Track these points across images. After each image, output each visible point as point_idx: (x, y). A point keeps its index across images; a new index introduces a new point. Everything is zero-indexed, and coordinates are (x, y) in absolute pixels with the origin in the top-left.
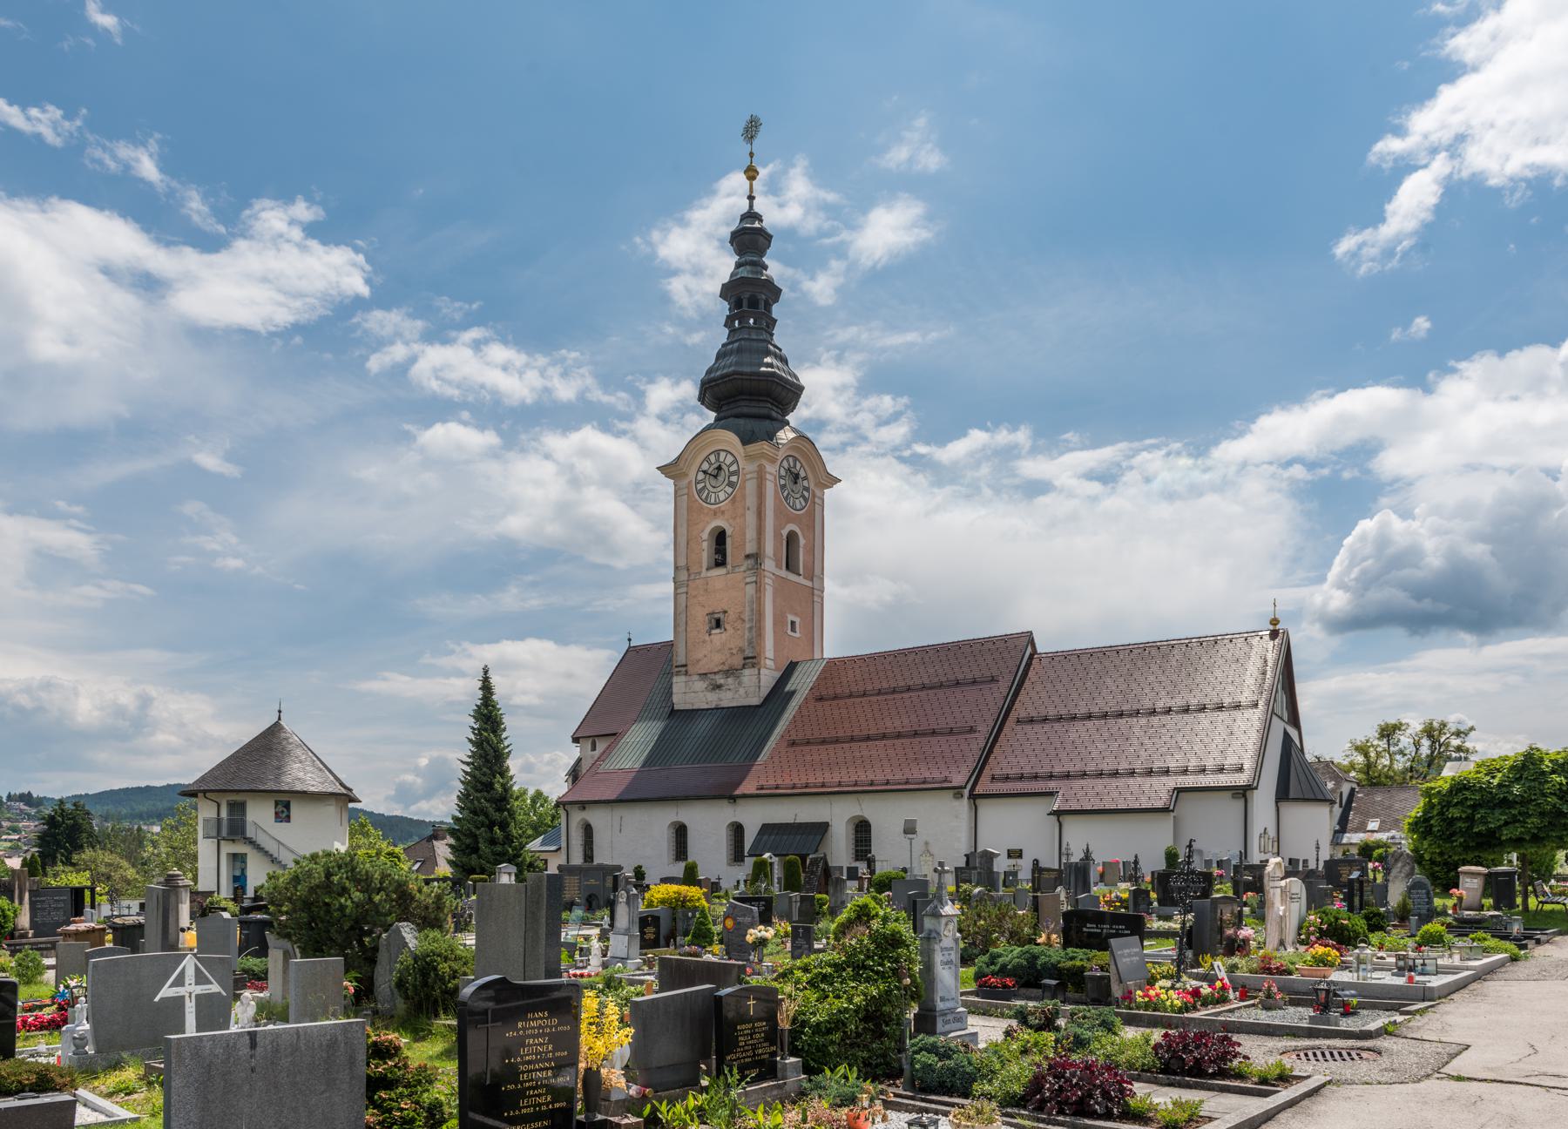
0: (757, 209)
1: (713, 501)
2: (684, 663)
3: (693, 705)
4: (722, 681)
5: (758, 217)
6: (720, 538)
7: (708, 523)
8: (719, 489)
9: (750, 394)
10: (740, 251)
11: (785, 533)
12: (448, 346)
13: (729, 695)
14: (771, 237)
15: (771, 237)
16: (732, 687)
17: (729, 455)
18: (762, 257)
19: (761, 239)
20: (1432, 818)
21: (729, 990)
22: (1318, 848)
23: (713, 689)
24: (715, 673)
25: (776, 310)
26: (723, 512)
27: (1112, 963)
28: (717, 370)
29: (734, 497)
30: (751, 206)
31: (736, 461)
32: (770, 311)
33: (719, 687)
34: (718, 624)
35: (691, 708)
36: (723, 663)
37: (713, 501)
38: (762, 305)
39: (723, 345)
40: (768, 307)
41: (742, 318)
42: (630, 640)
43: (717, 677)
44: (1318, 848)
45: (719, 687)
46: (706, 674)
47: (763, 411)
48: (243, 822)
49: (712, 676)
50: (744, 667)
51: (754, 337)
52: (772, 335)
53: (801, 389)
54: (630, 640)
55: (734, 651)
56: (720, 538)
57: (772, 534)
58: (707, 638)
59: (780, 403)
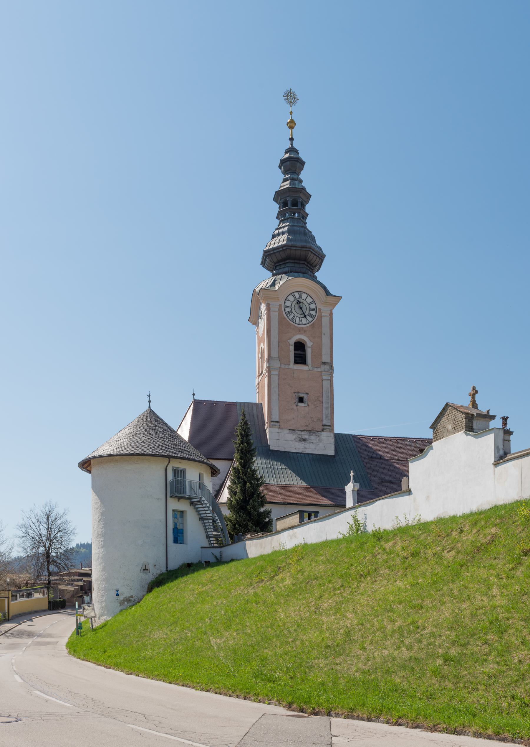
0: (295, 146)
2: (277, 420)
3: (284, 448)
4: (307, 437)
5: (296, 152)
6: (300, 346)
7: (294, 335)
9: (295, 259)
11: (292, 342)
13: (312, 446)
16: (314, 441)
17: (309, 297)
18: (298, 175)
19: (298, 164)
20: (88, 647)
23: (300, 441)
24: (301, 431)
25: (308, 208)
26: (305, 331)
29: (313, 324)
30: (292, 144)
31: (313, 302)
32: (304, 208)
33: (304, 440)
34: (301, 400)
35: (283, 450)
36: (307, 426)
37: (297, 322)
38: (299, 204)
40: (303, 206)
42: (194, 395)
43: (303, 433)
45: (304, 440)
46: (294, 430)
48: (184, 482)
49: (299, 432)
50: (323, 430)
51: (296, 224)
52: (306, 223)
54: (194, 395)
55: (315, 420)
56: (300, 346)
58: (295, 407)
59: (311, 265)
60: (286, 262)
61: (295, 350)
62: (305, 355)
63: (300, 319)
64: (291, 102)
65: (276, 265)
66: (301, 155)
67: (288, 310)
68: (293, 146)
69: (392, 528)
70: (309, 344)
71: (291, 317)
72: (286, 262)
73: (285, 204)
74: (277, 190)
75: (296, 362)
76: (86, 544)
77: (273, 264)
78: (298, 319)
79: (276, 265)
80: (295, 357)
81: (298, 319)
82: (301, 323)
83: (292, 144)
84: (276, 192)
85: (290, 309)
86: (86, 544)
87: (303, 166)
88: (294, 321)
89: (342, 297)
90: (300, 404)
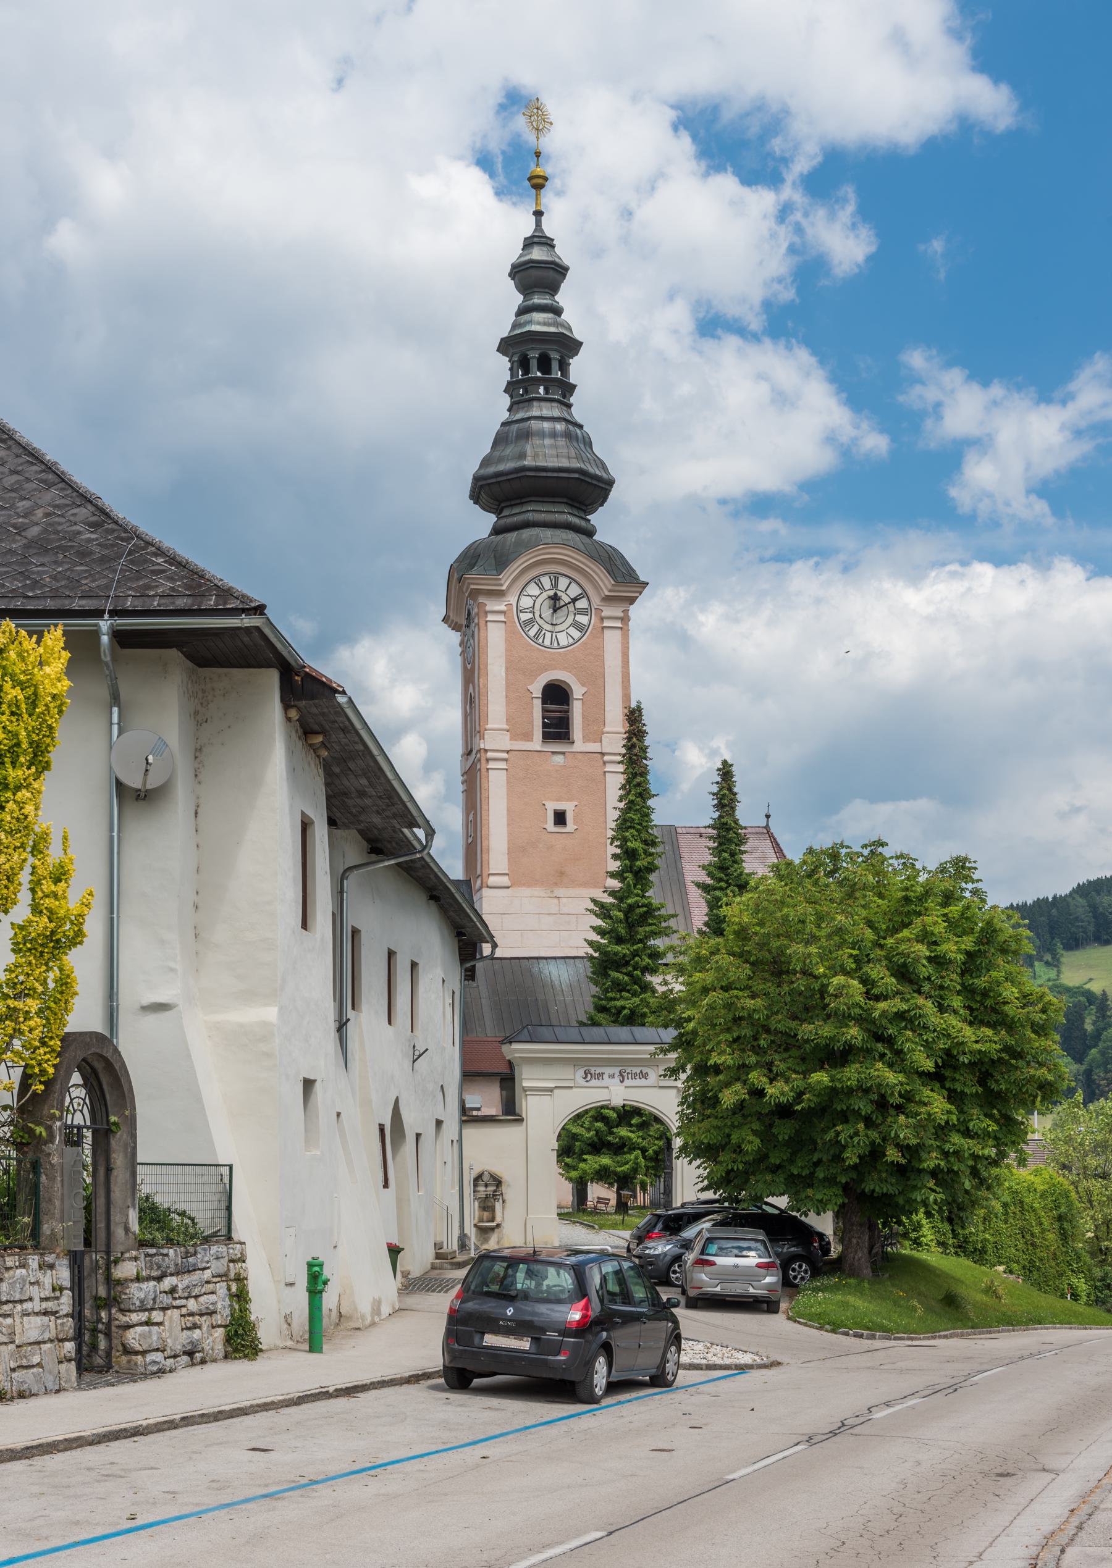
0: (549, 229)
1: (547, 642)
8: (558, 628)
10: (525, 289)
11: (537, 689)
12: (1013, 568)
14: (567, 269)
15: (567, 269)
17: (573, 585)
21: (627, 1193)
22: (196, 813)
27: (94, 928)
28: (500, 460)
30: (538, 224)
37: (547, 642)
39: (504, 424)
40: (564, 367)
41: (528, 384)
44: (196, 813)
47: (561, 510)
53: (611, 483)
57: (502, 662)
59: (580, 503)
60: (523, 501)
61: (544, 703)
62: (568, 718)
63: (554, 635)
64: (537, 129)
65: (503, 505)
66: (564, 253)
67: (524, 617)
68: (542, 231)
69: (64, 957)
70: (577, 691)
71: (532, 633)
72: (523, 501)
73: (524, 363)
74: (505, 334)
75: (547, 736)
76: (1050, 899)
77: (497, 503)
78: (548, 635)
79: (503, 505)
80: (545, 725)
81: (548, 635)
82: (556, 645)
83: (538, 224)
84: (502, 339)
85: (531, 615)
86: (1050, 899)
87: (564, 275)
88: (540, 641)
89: (647, 584)
90: (679, 315)
